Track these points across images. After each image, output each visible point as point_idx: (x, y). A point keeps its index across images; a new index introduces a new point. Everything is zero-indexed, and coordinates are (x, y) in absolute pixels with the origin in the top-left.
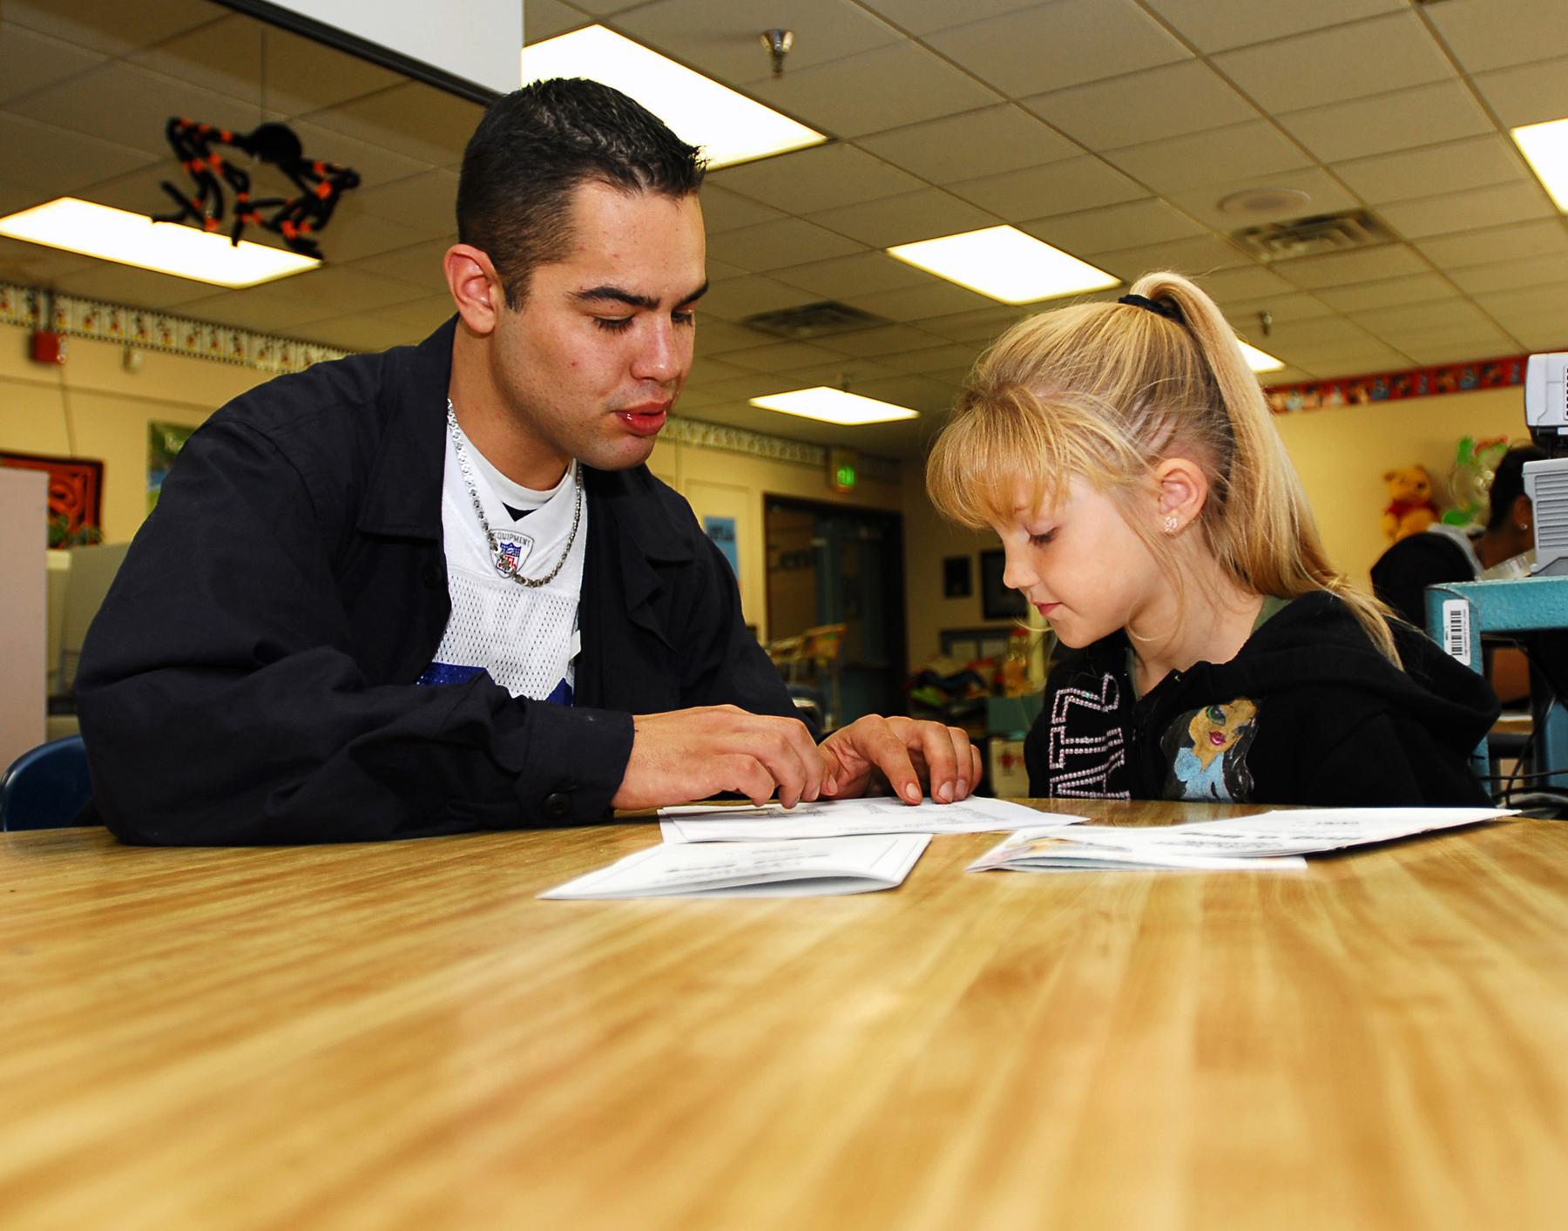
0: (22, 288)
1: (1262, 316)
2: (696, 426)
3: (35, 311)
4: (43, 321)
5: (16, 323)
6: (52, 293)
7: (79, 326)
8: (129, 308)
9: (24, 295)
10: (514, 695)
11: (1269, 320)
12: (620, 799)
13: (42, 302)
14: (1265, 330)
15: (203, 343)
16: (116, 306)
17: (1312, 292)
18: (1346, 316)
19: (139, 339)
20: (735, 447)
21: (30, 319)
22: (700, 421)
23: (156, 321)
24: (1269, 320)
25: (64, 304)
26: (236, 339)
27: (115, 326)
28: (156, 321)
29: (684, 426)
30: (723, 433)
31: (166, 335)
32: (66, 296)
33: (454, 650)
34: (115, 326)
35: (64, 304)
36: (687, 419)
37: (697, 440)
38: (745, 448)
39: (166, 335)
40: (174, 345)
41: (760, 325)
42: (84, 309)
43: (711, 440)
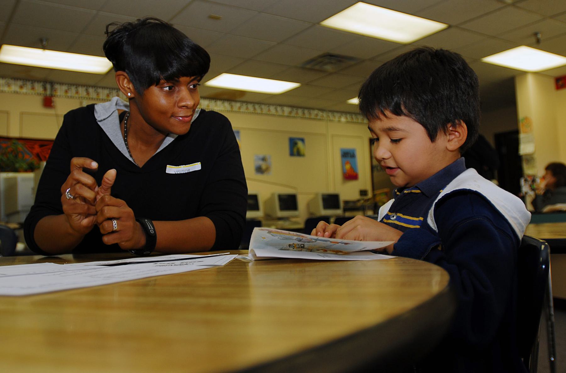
0: (40, 82)
1: (536, 34)
2: (336, 114)
3: (45, 89)
4: (48, 92)
5: (38, 94)
6: (52, 84)
7: (63, 93)
8: (83, 86)
9: (42, 84)
10: (251, 191)
11: (539, 36)
12: (401, 233)
13: (48, 86)
14: (538, 41)
15: (243, 109)
16: (77, 85)
17: (552, 17)
18: (457, 27)
19: (87, 96)
20: (355, 120)
21: (43, 92)
22: (337, 112)
23: (93, 90)
24: (539, 36)
25: (57, 86)
26: (87, 90)
27: (77, 93)
28: (93, 90)
29: (330, 114)
30: (348, 116)
31: (98, 94)
32: (57, 83)
33: (141, 166)
34: (77, 93)
35: (57, 86)
36: (330, 111)
37: (337, 119)
38: (360, 121)
39: (98, 94)
40: (101, 97)
41: (308, 66)
42: (65, 88)
43: (243, 110)
